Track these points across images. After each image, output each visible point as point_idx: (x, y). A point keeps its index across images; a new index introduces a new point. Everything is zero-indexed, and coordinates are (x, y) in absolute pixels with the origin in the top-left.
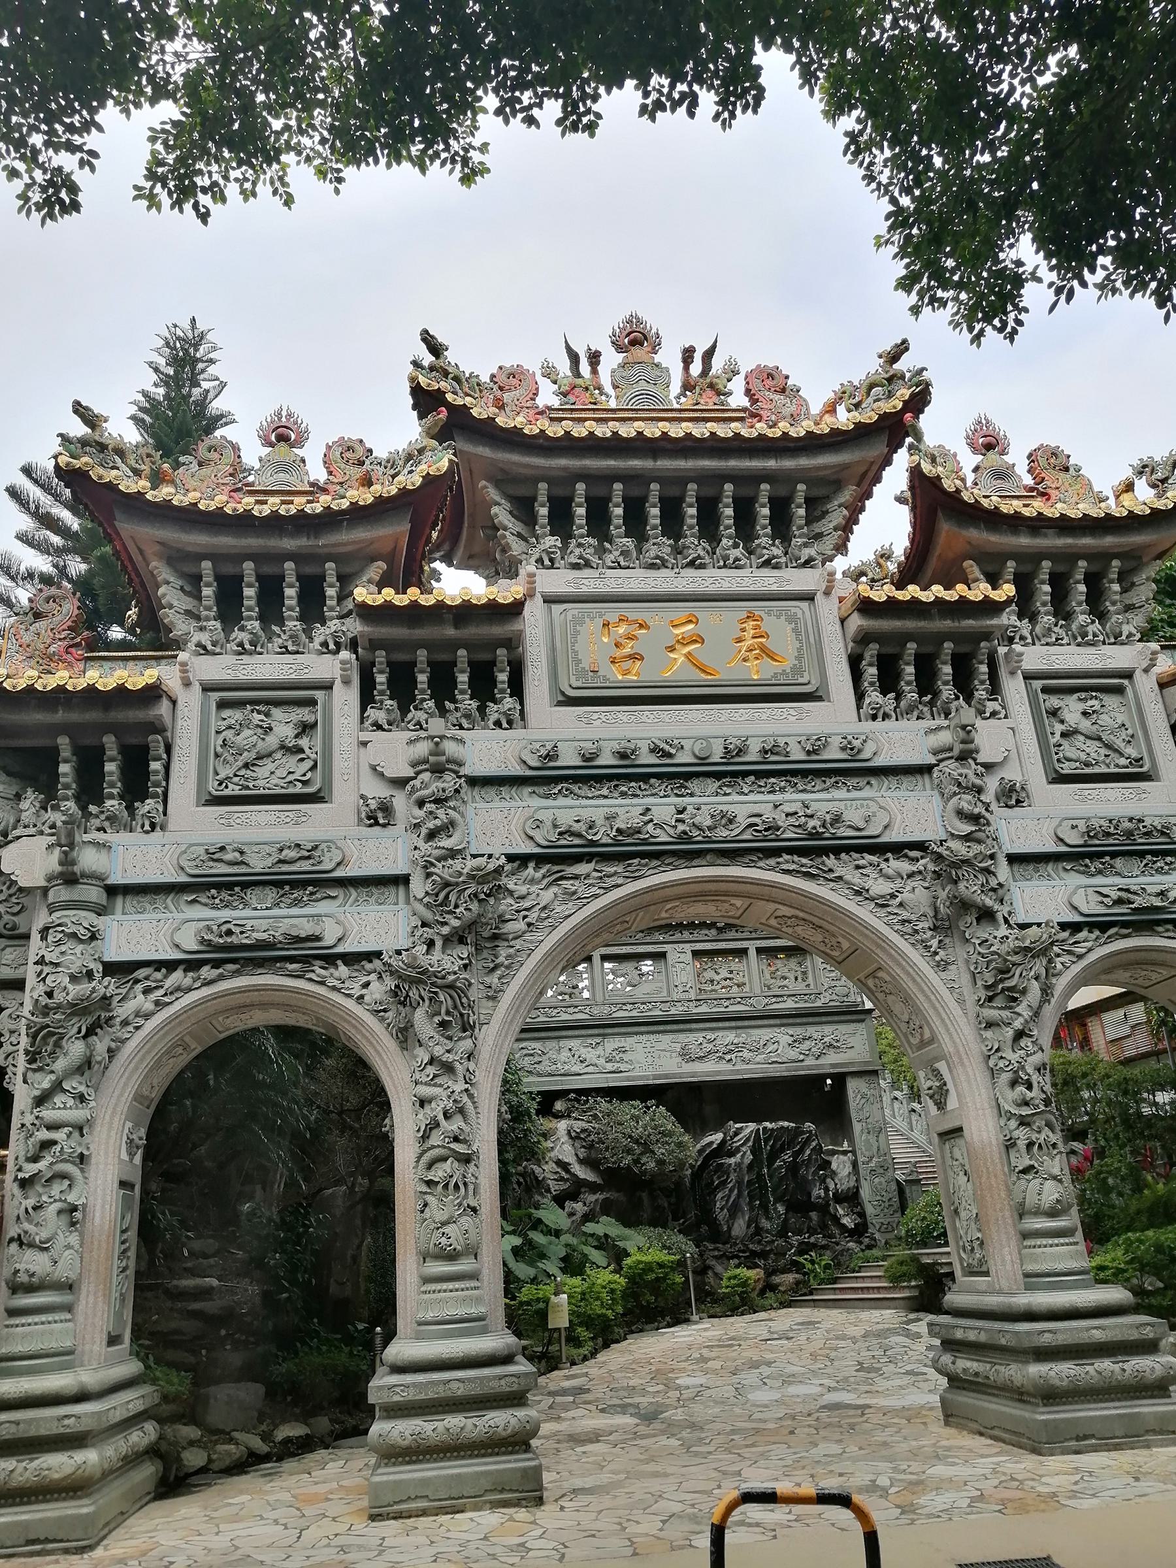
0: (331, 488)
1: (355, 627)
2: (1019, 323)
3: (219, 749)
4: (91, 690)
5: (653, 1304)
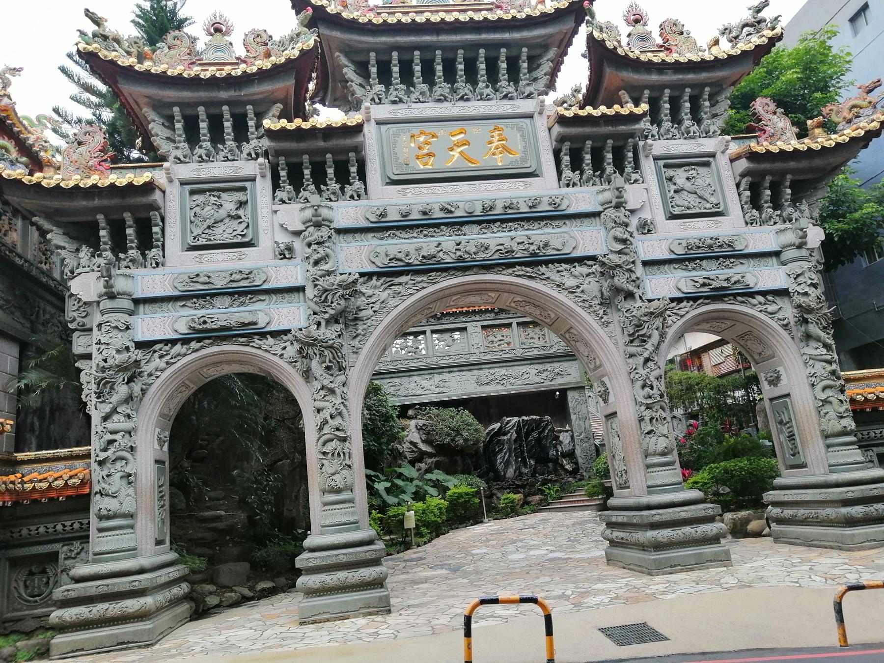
1: (266, 143)
4: (113, 186)
5: (462, 514)
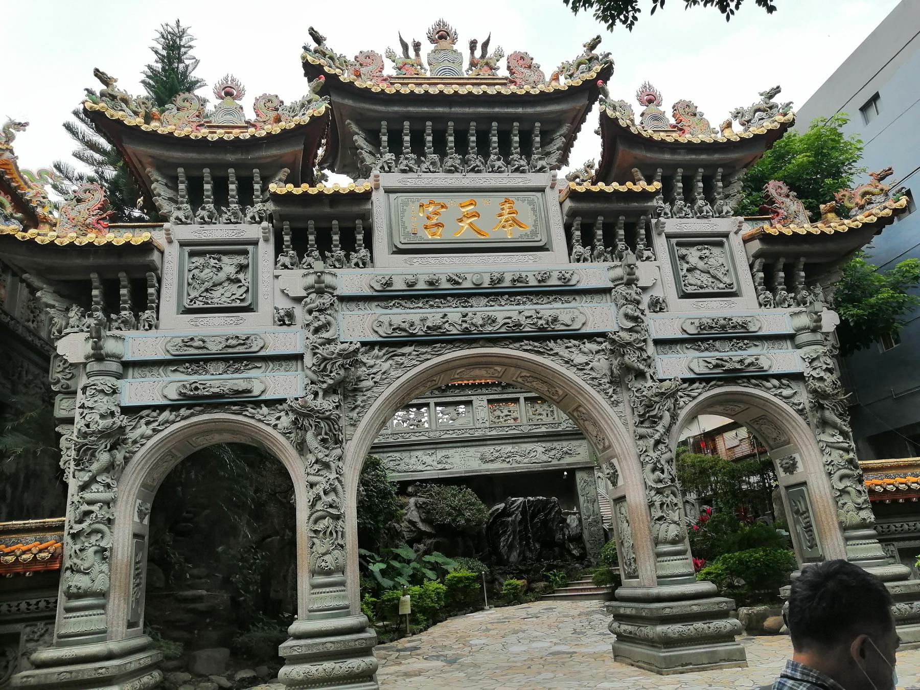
0: (258, 124)
1: (270, 207)
2: (635, 18)
3: (190, 281)
4: (109, 245)
5: (461, 600)
